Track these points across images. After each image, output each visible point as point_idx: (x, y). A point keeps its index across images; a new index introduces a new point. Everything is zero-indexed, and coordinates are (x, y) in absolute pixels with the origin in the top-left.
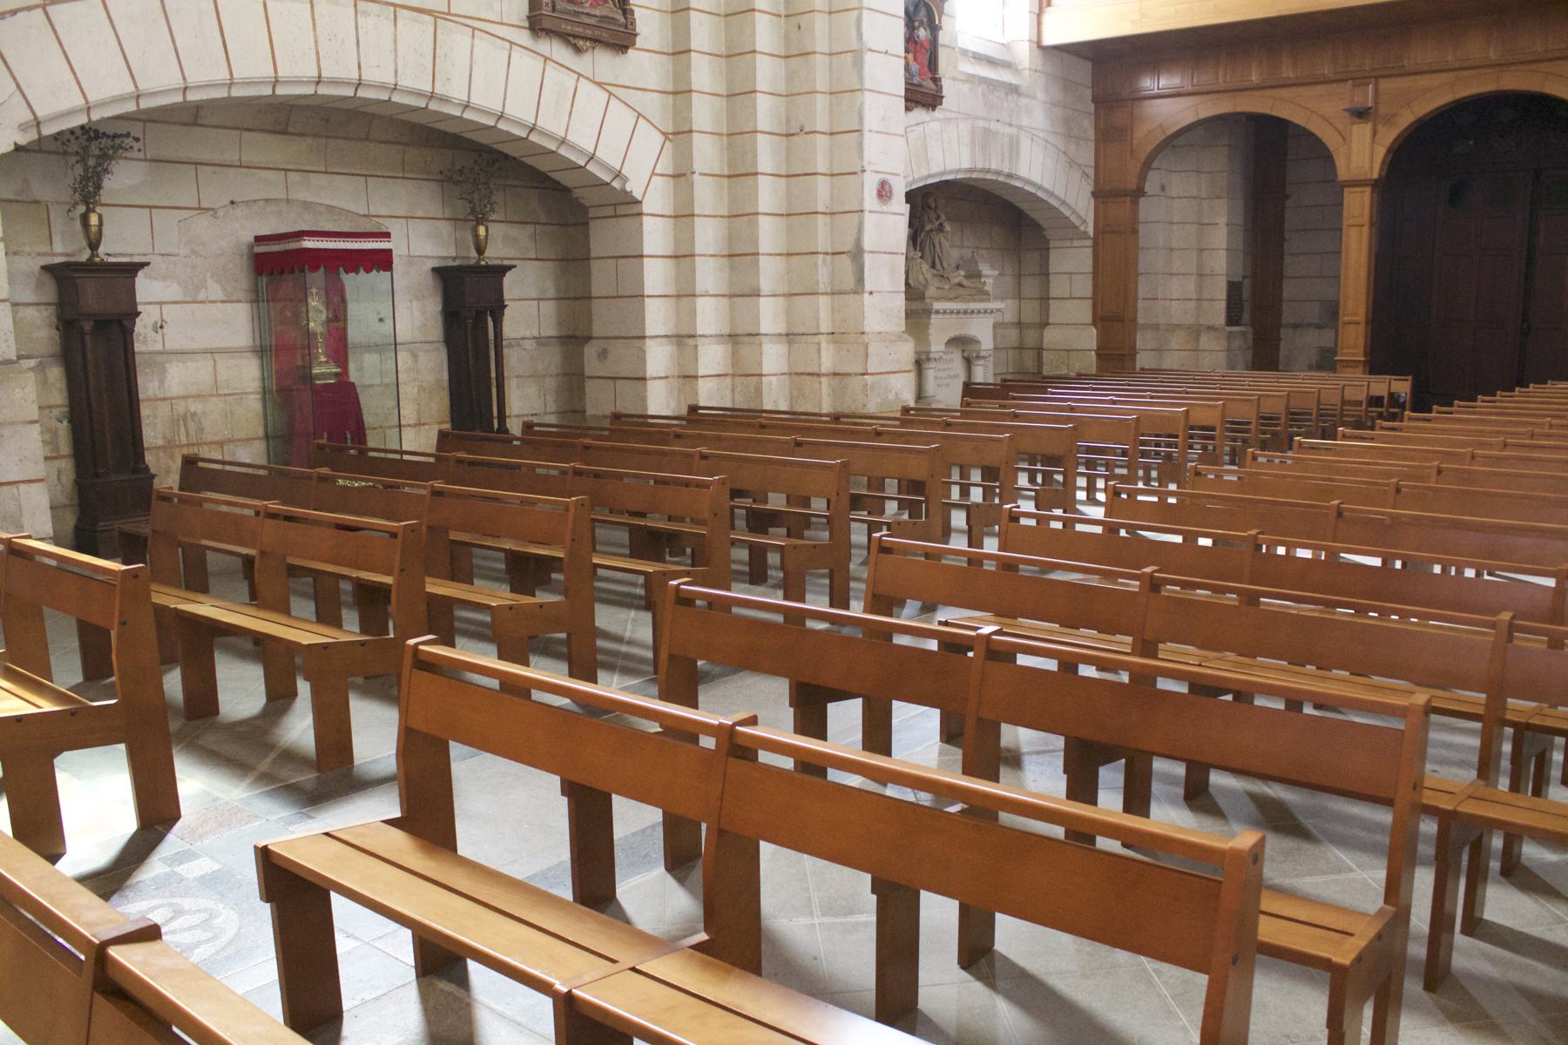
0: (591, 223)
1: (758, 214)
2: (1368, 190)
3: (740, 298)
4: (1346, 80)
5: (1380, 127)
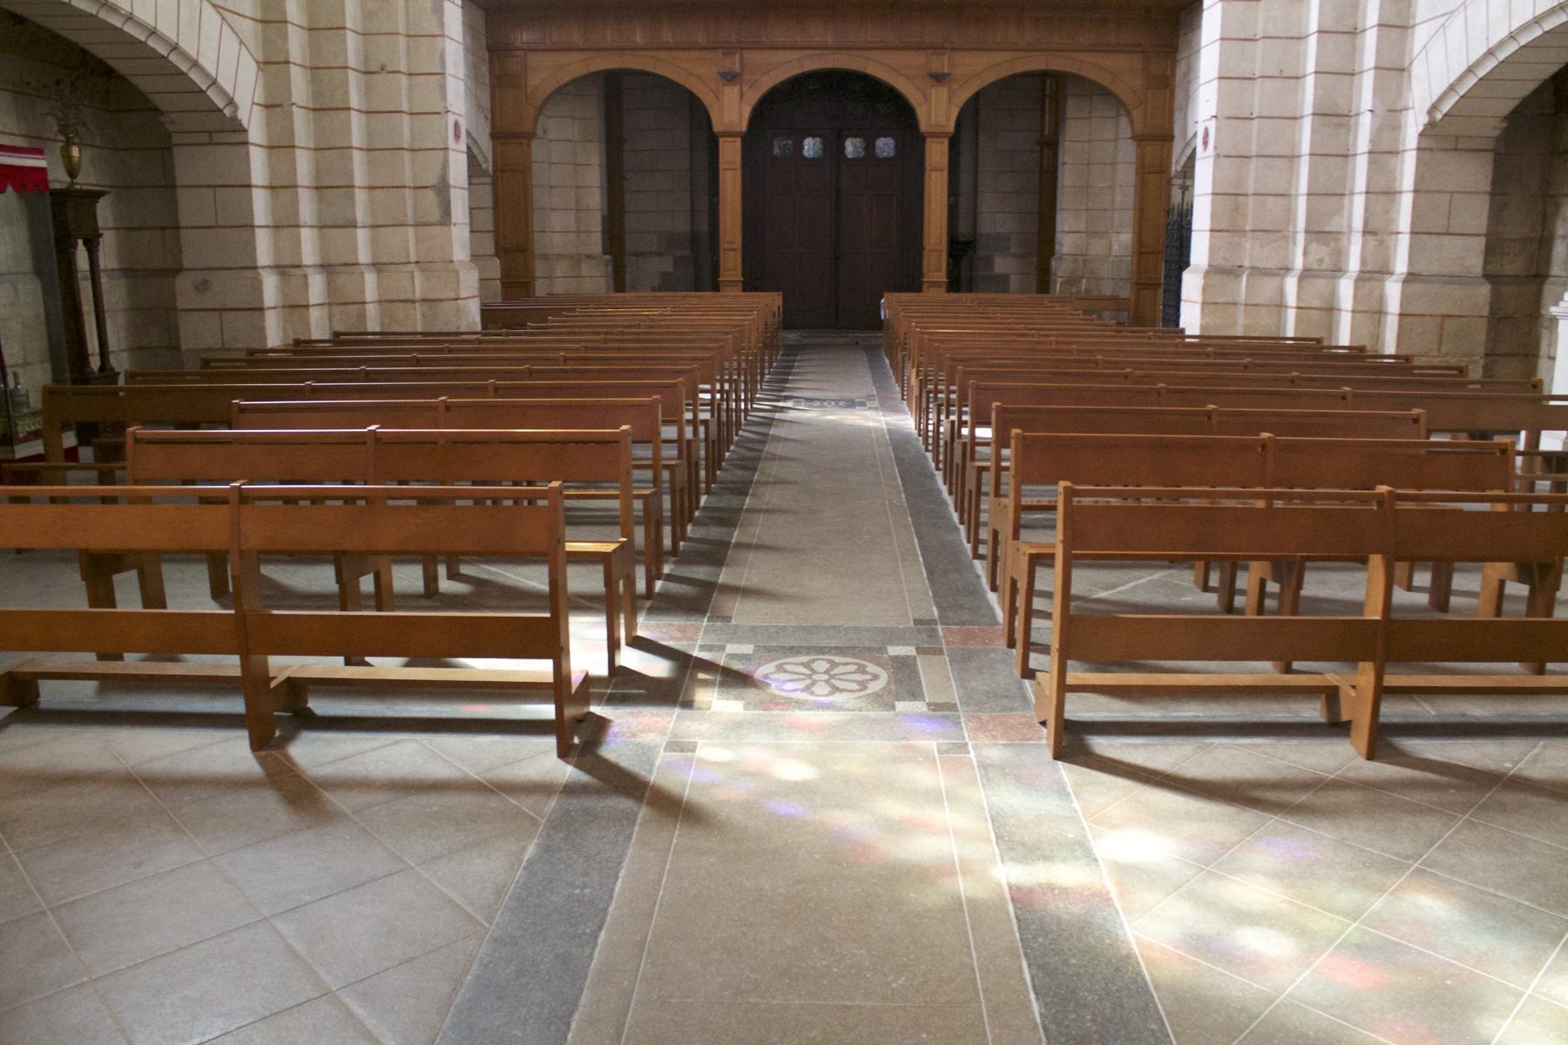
0: (176, 150)
2: (739, 140)
4: (716, 49)
5: (745, 89)
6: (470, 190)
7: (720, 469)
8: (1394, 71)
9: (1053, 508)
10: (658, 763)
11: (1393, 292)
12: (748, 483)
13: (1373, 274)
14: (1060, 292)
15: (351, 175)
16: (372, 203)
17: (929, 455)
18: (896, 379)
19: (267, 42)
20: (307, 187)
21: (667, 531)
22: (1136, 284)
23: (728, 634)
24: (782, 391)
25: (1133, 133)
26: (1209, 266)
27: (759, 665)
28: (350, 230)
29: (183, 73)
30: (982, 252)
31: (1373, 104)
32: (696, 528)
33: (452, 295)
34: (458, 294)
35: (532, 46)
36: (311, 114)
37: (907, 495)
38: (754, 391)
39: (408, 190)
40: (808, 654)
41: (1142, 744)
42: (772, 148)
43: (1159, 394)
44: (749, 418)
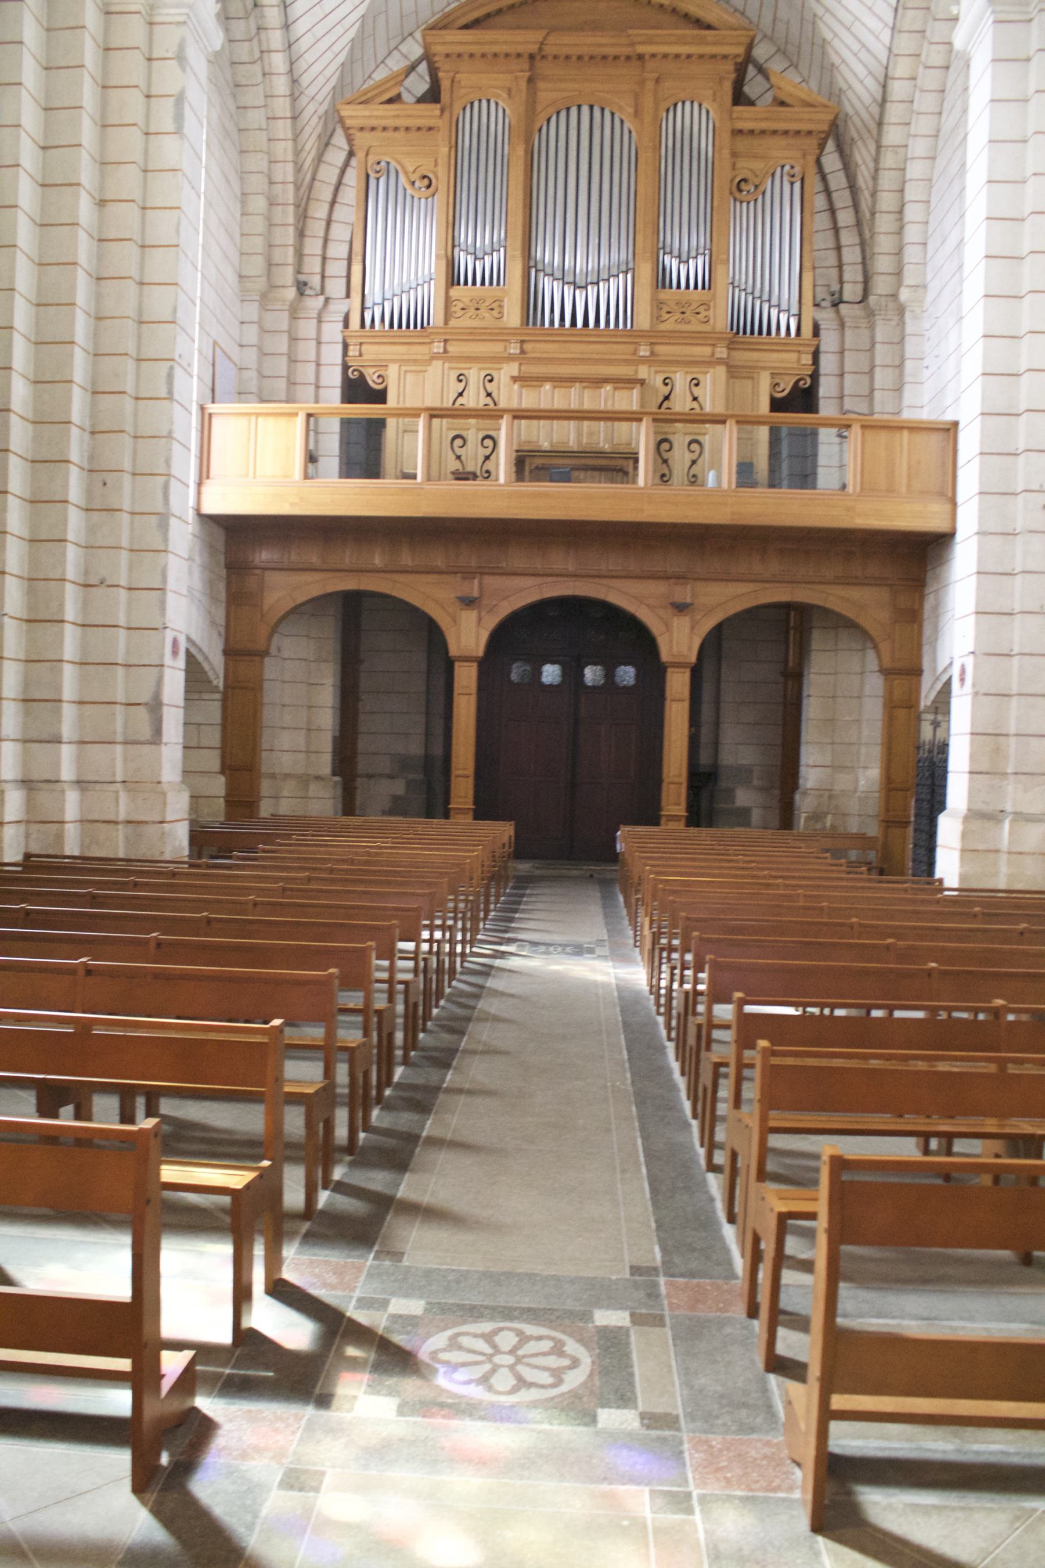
1: (62, 661)
2: (475, 665)
3: (38, 745)
4: (456, 573)
5: (483, 614)
6: (186, 708)
7: (424, 1030)
9: (812, 1216)
10: (264, 1512)
12: (452, 1052)
14: (806, 828)
15: (59, 688)
16: (81, 718)
17: (661, 1019)
18: (630, 920)
20: (14, 700)
21: (341, 1116)
22: (884, 821)
23: (395, 1281)
24: (506, 932)
25: (881, 666)
26: (969, 810)
27: (428, 1336)
28: (57, 745)
30: (723, 784)
32: (384, 1113)
33: (160, 819)
34: (164, 817)
35: (270, 565)
36: (24, 625)
37: (633, 1074)
38: (475, 930)
39: (118, 707)
40: (492, 1319)
41: (934, 1507)
42: (509, 672)
43: (929, 975)
44: (466, 964)
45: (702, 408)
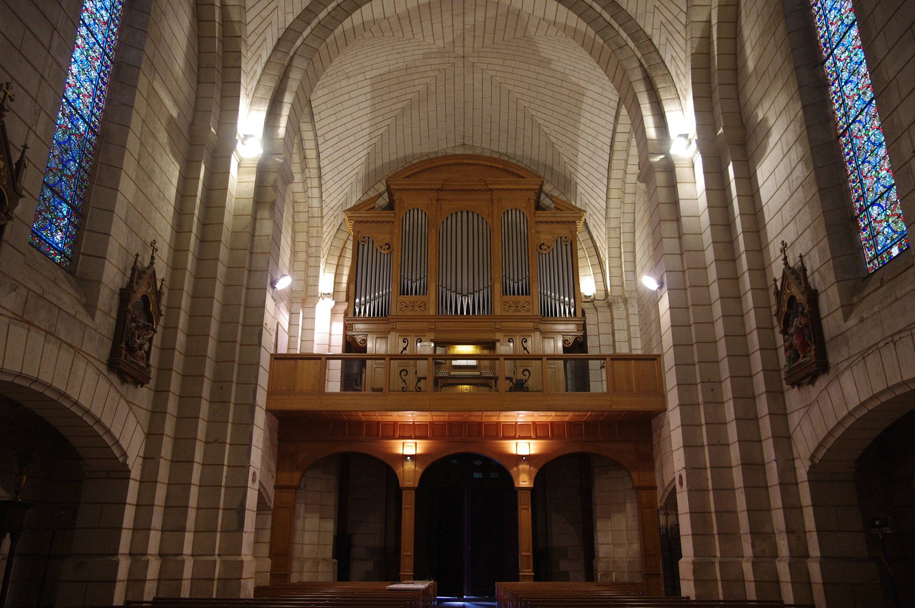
2: (413, 491)
8: (783, 438)
11: (815, 570)
13: (799, 556)
19: (152, 422)
29: (100, 436)
31: (776, 456)
45: (528, 352)
